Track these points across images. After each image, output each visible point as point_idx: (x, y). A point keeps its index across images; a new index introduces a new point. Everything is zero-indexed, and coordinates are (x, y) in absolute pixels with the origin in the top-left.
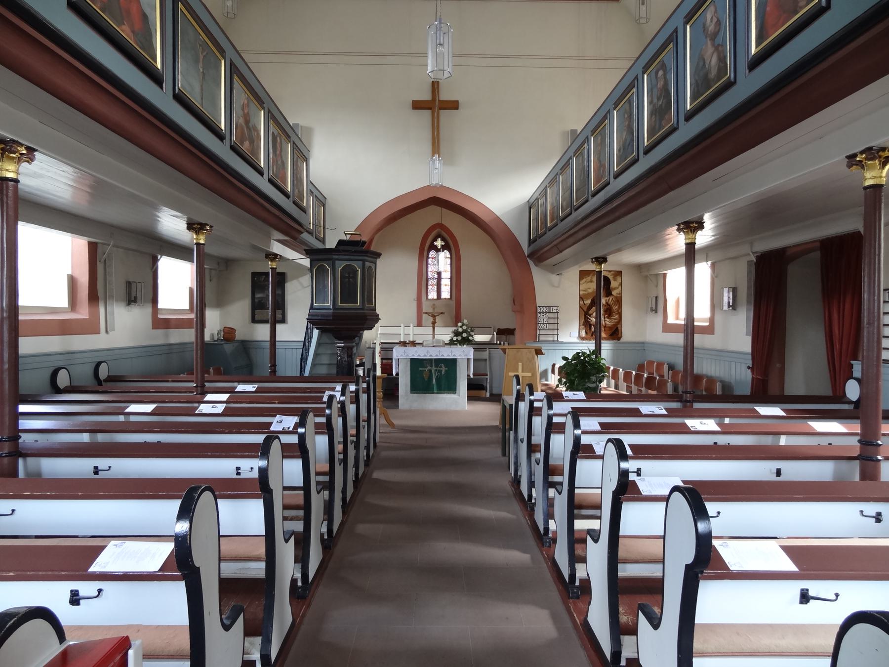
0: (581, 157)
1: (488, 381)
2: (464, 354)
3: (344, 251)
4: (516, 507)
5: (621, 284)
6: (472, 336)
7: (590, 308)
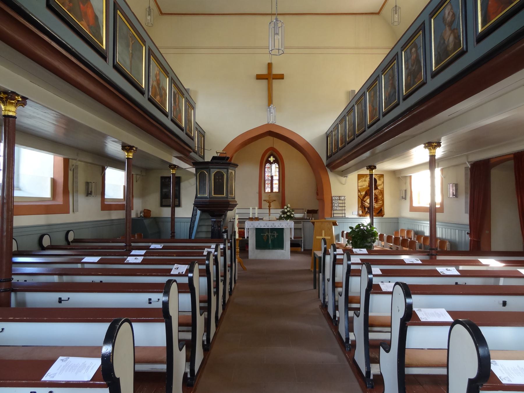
0: (360, 105)
1: (303, 242)
2: (288, 225)
3: (216, 163)
4: (325, 322)
5: (383, 183)
6: (293, 214)
7: (364, 197)
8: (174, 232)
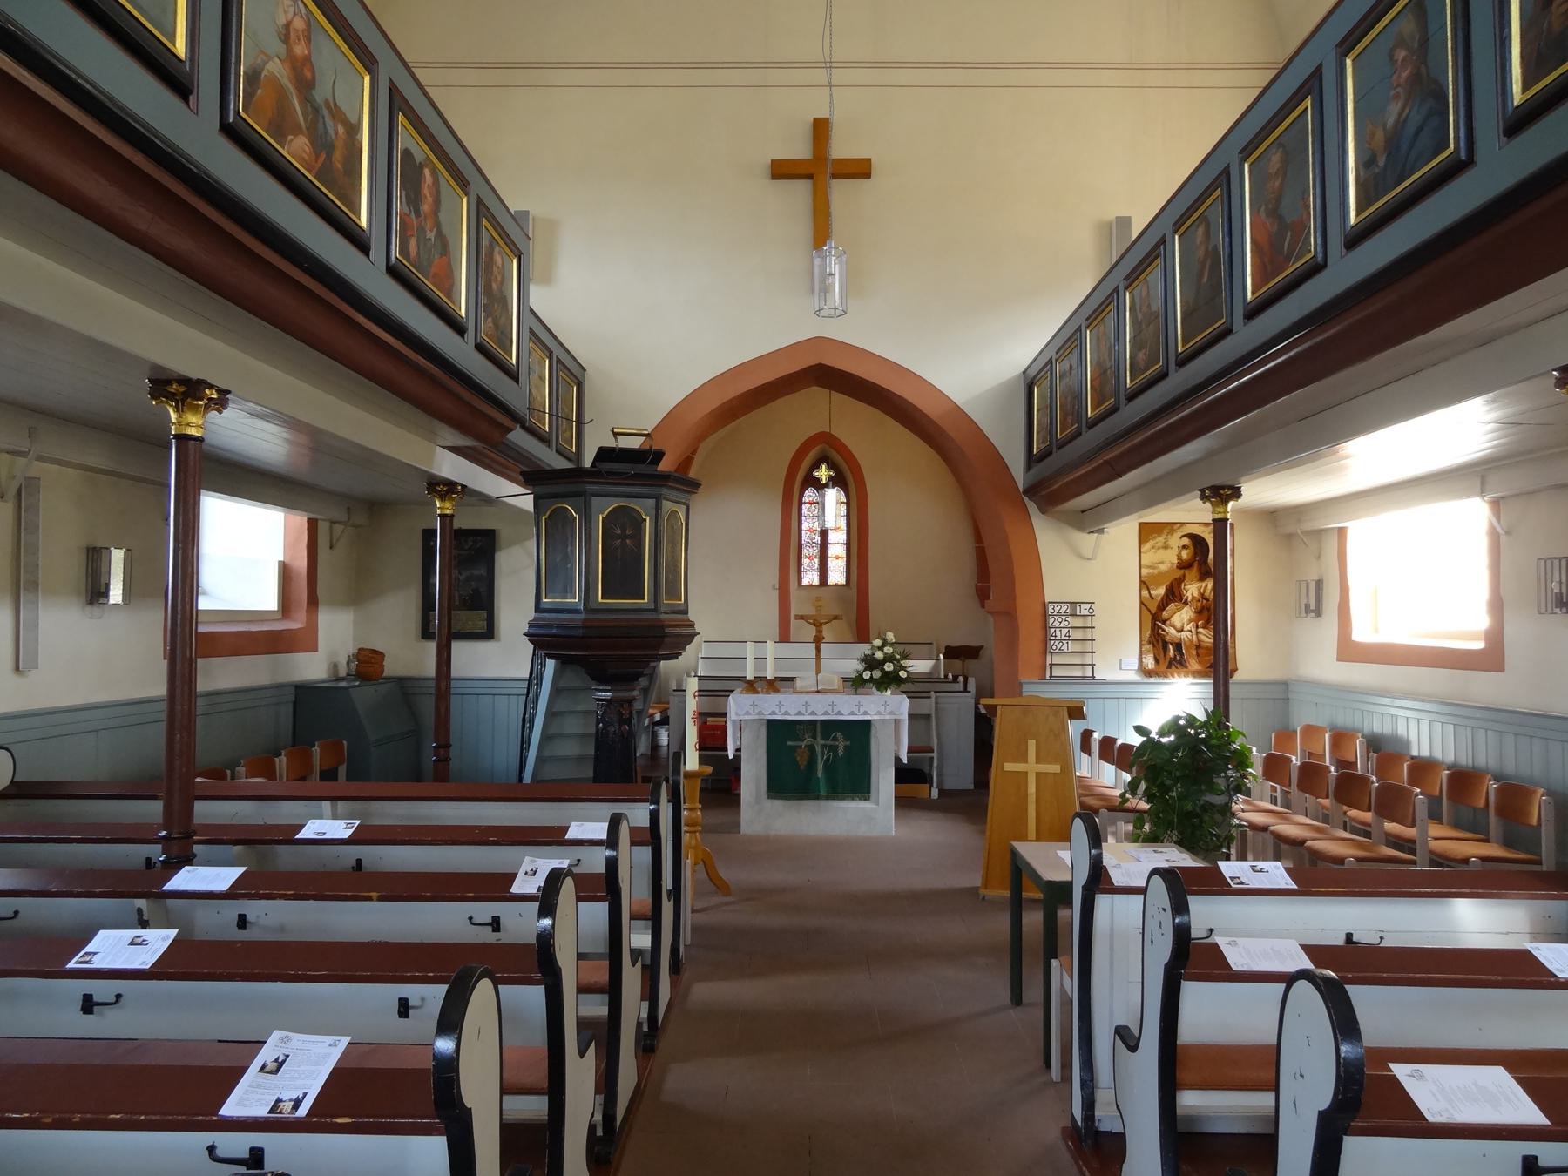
1: (935, 764)
7: (1163, 605)
8: (447, 746)
